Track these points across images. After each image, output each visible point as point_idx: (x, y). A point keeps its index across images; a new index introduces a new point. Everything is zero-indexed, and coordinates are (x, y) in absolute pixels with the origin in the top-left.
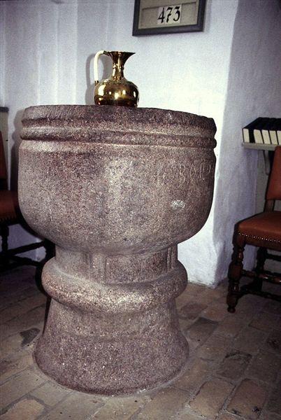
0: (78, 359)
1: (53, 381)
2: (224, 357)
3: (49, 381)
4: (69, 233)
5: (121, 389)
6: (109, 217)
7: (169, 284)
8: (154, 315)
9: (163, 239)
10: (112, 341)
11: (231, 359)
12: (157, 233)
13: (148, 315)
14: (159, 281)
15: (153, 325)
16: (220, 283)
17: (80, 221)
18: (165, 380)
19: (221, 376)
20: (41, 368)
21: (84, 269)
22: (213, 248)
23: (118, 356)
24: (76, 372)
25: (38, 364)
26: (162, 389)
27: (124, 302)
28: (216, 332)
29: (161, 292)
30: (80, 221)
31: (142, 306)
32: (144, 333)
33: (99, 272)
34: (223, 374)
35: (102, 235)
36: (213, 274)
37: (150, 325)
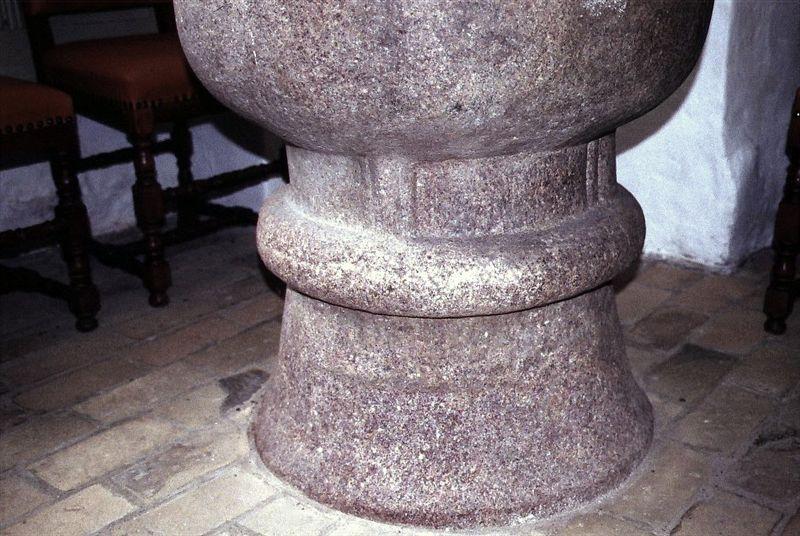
0: (354, 436)
1: (297, 492)
2: (749, 444)
3: (285, 493)
4: (305, 97)
5: (469, 514)
6: (409, 42)
7: (589, 239)
8: (553, 321)
9: (567, 107)
10: (441, 389)
11: (771, 449)
12: (546, 88)
13: (534, 322)
14: (563, 231)
15: (550, 350)
16: (743, 260)
17: (331, 58)
18: (587, 494)
19: (741, 491)
20: (266, 461)
21: (357, 203)
22: (723, 162)
23: (457, 429)
24: (351, 471)
25: (261, 453)
26: (577, 518)
27: (466, 285)
28: (730, 381)
29: (566, 257)
30: (331, 58)
31: (517, 295)
32: (525, 370)
33: (398, 206)
34: (748, 485)
35: (391, 96)
36: (724, 237)
37: (543, 350)
